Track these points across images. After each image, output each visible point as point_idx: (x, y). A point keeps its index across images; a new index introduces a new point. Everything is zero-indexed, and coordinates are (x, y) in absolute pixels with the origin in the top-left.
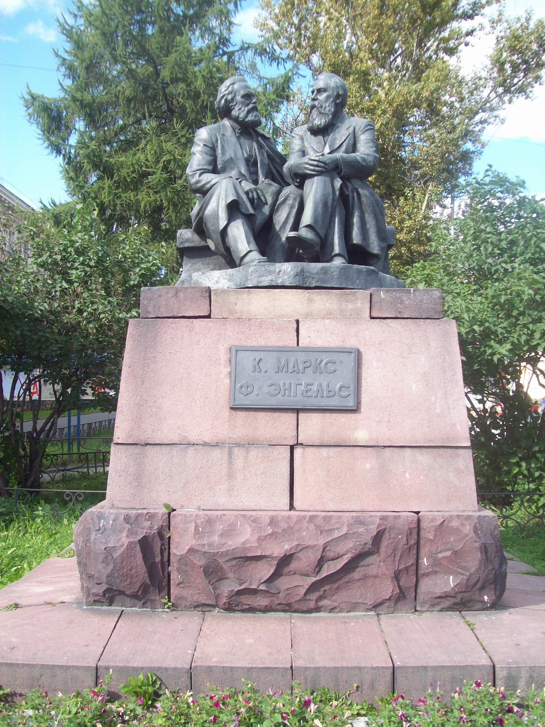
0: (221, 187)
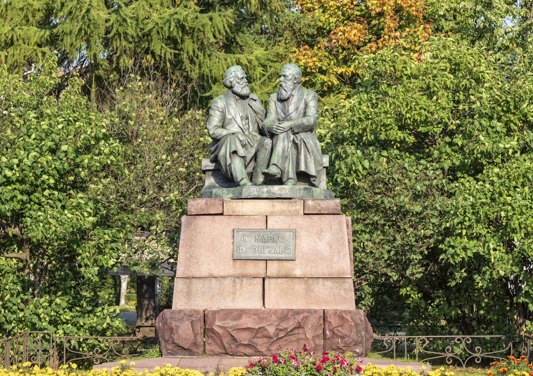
0: (318, 152)
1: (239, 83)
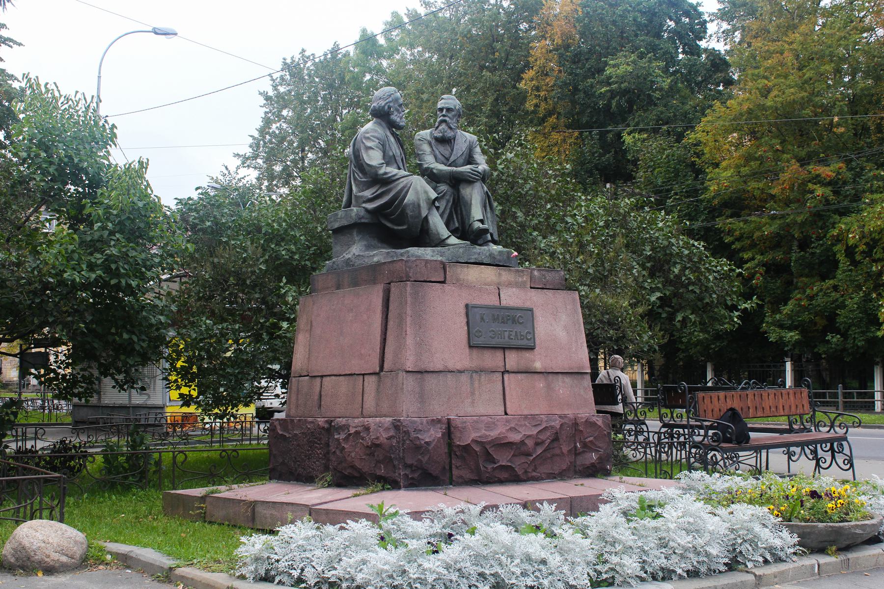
1: (398, 111)
